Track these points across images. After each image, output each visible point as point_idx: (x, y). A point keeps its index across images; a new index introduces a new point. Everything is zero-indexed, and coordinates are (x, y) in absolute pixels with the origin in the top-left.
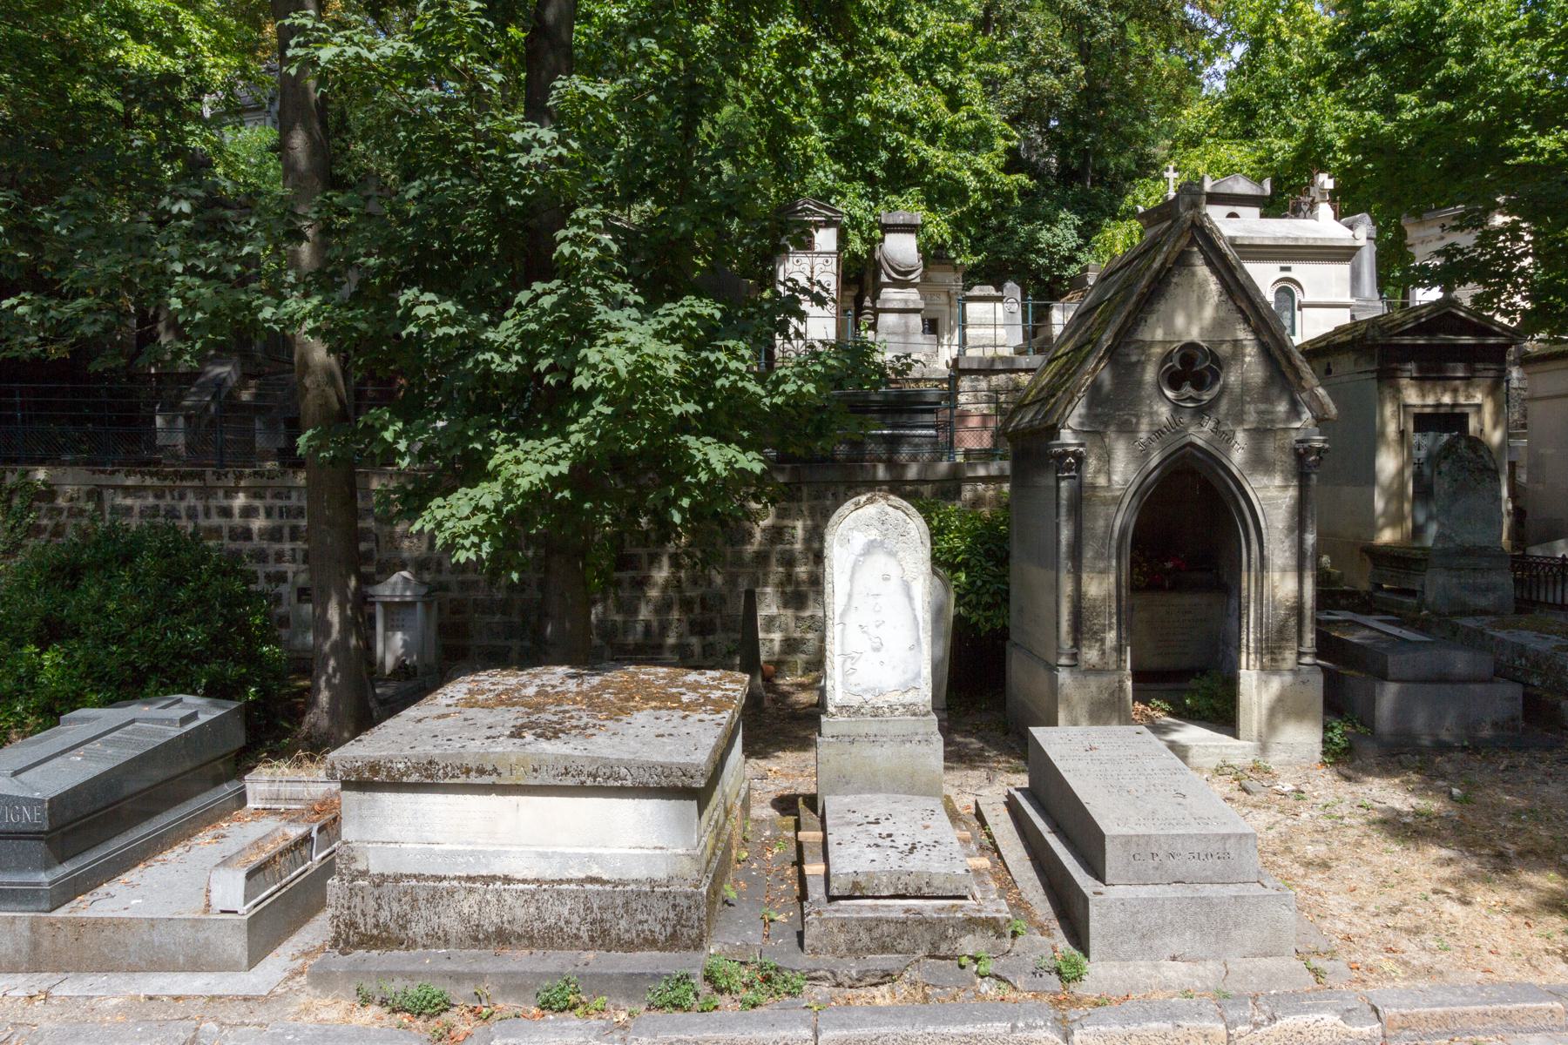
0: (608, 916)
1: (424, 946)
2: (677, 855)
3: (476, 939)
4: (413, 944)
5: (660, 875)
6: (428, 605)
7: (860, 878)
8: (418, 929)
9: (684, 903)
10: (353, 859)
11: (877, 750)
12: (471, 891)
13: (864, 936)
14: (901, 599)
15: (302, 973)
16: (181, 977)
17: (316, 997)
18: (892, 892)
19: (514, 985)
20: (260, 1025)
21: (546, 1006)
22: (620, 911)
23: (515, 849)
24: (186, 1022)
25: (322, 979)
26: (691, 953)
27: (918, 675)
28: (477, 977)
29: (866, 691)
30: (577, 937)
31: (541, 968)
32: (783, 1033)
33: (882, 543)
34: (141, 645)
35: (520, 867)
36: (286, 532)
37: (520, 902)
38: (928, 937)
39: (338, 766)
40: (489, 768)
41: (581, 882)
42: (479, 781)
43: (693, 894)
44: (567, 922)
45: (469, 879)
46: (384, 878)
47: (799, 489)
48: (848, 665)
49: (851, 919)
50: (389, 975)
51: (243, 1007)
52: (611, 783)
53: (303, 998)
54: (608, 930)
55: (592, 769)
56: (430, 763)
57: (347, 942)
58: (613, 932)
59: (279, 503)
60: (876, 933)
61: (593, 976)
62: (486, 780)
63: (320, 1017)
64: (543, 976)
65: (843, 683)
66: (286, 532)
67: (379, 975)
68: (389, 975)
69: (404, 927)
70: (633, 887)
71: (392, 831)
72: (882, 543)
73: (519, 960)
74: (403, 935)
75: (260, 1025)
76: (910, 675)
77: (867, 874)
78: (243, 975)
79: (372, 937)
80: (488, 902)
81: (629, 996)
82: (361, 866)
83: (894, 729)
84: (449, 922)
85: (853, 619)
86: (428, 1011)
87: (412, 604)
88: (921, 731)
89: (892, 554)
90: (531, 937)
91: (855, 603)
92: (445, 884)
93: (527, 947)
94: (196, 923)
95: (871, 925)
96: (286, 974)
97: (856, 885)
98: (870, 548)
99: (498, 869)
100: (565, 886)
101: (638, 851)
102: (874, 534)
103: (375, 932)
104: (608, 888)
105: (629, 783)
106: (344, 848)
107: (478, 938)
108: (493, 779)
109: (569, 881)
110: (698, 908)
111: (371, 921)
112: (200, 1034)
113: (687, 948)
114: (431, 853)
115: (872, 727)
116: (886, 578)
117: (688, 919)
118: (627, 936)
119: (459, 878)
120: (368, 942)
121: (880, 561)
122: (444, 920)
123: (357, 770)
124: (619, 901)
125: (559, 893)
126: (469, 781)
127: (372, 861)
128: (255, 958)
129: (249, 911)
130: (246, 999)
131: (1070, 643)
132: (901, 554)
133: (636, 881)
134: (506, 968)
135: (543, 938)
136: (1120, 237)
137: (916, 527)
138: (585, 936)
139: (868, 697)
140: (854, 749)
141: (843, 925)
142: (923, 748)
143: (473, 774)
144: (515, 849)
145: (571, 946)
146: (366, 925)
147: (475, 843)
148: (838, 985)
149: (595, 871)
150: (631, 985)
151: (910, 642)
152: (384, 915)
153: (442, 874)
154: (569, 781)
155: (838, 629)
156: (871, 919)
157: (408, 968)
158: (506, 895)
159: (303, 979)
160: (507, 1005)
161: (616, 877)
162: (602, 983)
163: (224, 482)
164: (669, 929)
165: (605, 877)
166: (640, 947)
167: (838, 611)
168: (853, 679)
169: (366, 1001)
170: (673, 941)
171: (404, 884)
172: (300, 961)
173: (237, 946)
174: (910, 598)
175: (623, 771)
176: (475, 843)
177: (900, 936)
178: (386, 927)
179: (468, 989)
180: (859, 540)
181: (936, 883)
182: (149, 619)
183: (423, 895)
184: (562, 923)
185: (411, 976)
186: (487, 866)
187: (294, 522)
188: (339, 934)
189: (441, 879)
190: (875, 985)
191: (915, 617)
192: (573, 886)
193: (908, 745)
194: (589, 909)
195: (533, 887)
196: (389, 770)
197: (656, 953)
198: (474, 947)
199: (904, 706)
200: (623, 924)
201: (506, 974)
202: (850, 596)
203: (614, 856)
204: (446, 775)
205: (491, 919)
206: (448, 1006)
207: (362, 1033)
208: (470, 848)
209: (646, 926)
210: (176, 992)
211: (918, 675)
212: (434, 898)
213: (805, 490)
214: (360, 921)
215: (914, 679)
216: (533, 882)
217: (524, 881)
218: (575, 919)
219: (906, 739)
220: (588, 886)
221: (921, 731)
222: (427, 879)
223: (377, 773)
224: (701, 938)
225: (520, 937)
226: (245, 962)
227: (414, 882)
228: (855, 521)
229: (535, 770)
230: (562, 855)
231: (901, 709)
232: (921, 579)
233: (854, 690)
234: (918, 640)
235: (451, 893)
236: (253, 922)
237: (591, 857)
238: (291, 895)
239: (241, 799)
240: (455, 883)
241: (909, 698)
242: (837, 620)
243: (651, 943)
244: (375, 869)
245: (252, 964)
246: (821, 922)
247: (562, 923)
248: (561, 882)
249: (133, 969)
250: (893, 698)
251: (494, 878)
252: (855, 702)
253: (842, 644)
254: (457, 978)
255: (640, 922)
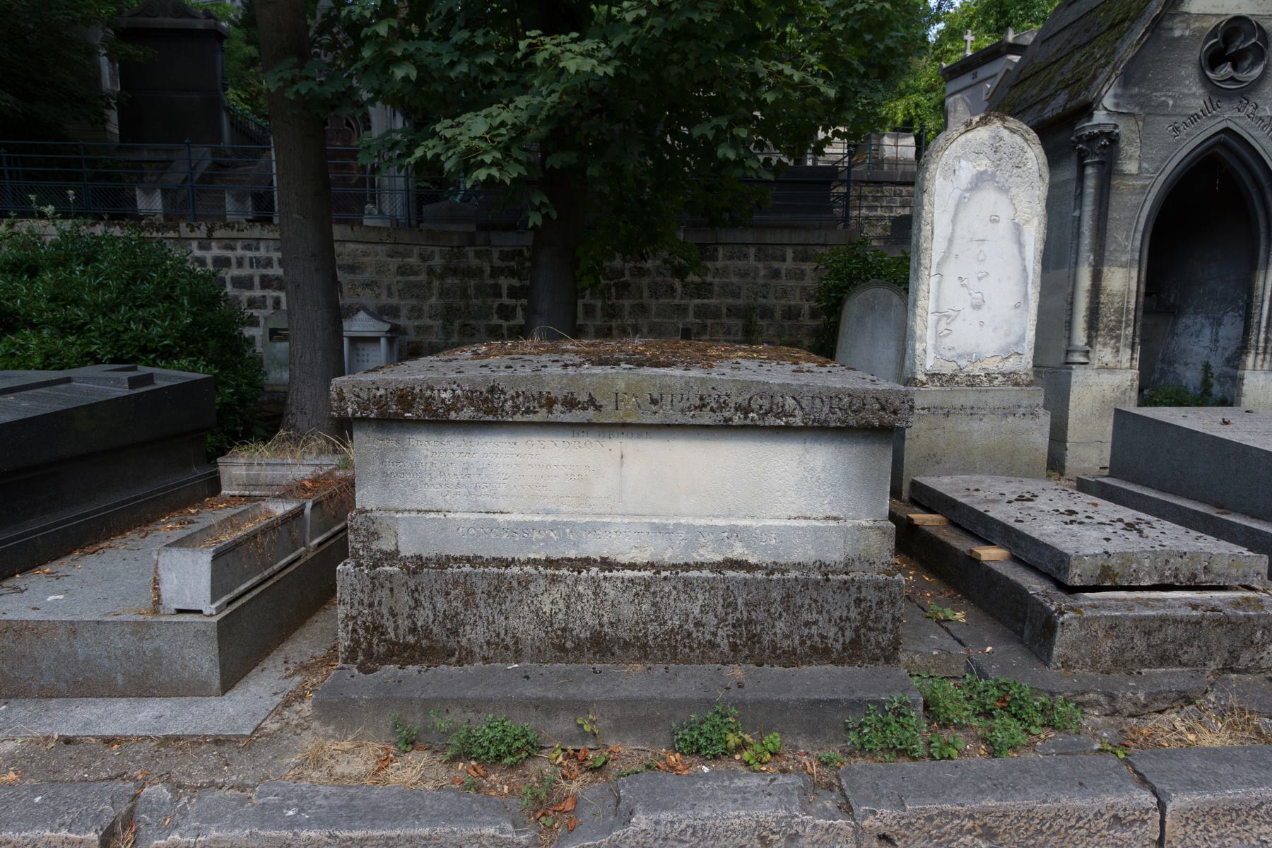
0: (759, 615)
1: (485, 659)
2: (861, 528)
3: (562, 648)
4: (466, 657)
5: (835, 556)
6: (390, 341)
7: (1113, 562)
8: (475, 635)
9: (871, 595)
10: (375, 535)
11: (975, 425)
12: (554, 580)
13: (1140, 643)
14: (1010, 247)
15: (302, 698)
16: (121, 705)
17: (327, 737)
18: (1155, 580)
19: (635, 717)
20: (242, 787)
21: (696, 751)
22: (777, 608)
23: (618, 520)
24: (119, 785)
25: (336, 711)
26: (881, 667)
27: (1022, 338)
28: (578, 706)
29: (960, 356)
30: (712, 645)
31: (674, 693)
32: (1110, 800)
33: (993, 175)
34: (102, 335)
35: (625, 547)
36: (257, 281)
37: (629, 596)
38: (1226, 643)
39: (347, 395)
40: (584, 398)
41: (717, 567)
42: (567, 418)
43: (887, 584)
44: (698, 624)
45: (549, 562)
46: (420, 563)
47: (716, 250)
48: (943, 325)
49: (1126, 618)
50: (444, 705)
51: (212, 757)
52: (771, 421)
53: (308, 741)
54: (759, 636)
55: (742, 400)
56: (492, 390)
57: (369, 654)
58: (766, 639)
59: (249, 254)
60: (1156, 639)
61: (759, 703)
62: (577, 416)
63: (338, 770)
64: (687, 704)
65: (935, 347)
66: (257, 281)
67: (426, 705)
68: (444, 705)
69: (454, 632)
70: (792, 574)
71: (433, 494)
72: (993, 175)
73: (633, 680)
74: (452, 643)
75: (242, 787)
76: (1013, 338)
77: (1122, 555)
78: (214, 702)
79: (407, 646)
80: (580, 596)
81: (814, 732)
82: (387, 546)
83: (993, 400)
84: (522, 624)
85: (951, 271)
86: (508, 760)
87: (376, 340)
88: (1025, 403)
89: (1004, 190)
90: (645, 646)
91: (955, 250)
92: (515, 570)
93: (637, 660)
94: (139, 629)
95: (1148, 627)
96: (278, 699)
97: (1106, 571)
98: (979, 181)
99: (594, 548)
100: (694, 574)
101: (803, 523)
102: (984, 164)
103: (411, 639)
104: (759, 575)
105: (798, 421)
106: (360, 519)
107: (566, 646)
108: (590, 414)
109: (699, 566)
110: (893, 604)
111: (404, 624)
112: (141, 806)
113: (874, 659)
114: (493, 526)
115: (968, 398)
116: (994, 220)
117: (877, 620)
118: (785, 644)
119: (534, 562)
120: (402, 653)
121: (989, 199)
122: (513, 622)
123: (378, 402)
124: (776, 594)
125: (687, 583)
126: (552, 418)
127: (403, 539)
128: (230, 680)
129: (219, 610)
130: (218, 741)
131: (1085, 340)
132: (1014, 191)
133: (798, 566)
134: (622, 693)
135: (661, 647)
136: (901, 107)
137: (1034, 155)
138: (724, 644)
139: (963, 363)
140: (948, 424)
141: (1113, 626)
142: (1026, 423)
143: (558, 407)
144: (618, 520)
145: (704, 659)
146: (398, 629)
147: (558, 512)
148: (1114, 713)
149: (738, 551)
150: (817, 717)
151: (1017, 298)
152: (424, 616)
153: (508, 555)
154: (706, 418)
155: (934, 280)
156: (1153, 619)
157: (469, 694)
158: (607, 586)
159: (306, 707)
160: (626, 748)
161: (769, 560)
162: (764, 714)
163: (197, 234)
164: (849, 634)
165: (753, 560)
166: (806, 659)
167: (936, 258)
168: (947, 342)
169: (411, 743)
170: (854, 651)
171: (453, 570)
172: (298, 679)
173: (204, 660)
174: (1020, 245)
175: (790, 402)
176: (558, 512)
177: (1189, 642)
178: (428, 633)
179: (563, 724)
180: (967, 170)
181: (1216, 568)
182: (113, 307)
183: (482, 586)
184: (690, 626)
185: (475, 705)
186: (575, 545)
187: (264, 272)
188: (356, 642)
189: (508, 563)
190: (1160, 712)
191: (1025, 269)
192: (706, 573)
193: (1010, 419)
194: (730, 605)
195: (647, 574)
196: (428, 402)
197: (830, 667)
198: (559, 660)
199: (1004, 375)
200: (781, 626)
201: (622, 702)
202: (951, 241)
203: (767, 530)
204: (516, 408)
205: (585, 618)
206: (533, 749)
207: (410, 805)
208: (550, 518)
209: (814, 630)
210: (108, 731)
211: (1022, 338)
212: (498, 589)
213: (721, 250)
214: (389, 623)
215: (1017, 344)
216: (645, 567)
217: (632, 566)
218: (711, 620)
219: (1008, 412)
220: (730, 574)
221: (1025, 403)
222: (486, 563)
223: (409, 406)
224: (896, 645)
225: (626, 645)
226: (216, 682)
227: (467, 568)
228: (963, 148)
229: (654, 402)
230: (690, 528)
231: (1001, 378)
232: (1035, 222)
233: (948, 354)
234: (1026, 296)
235: (525, 582)
236: (226, 628)
237: (735, 532)
238: (280, 596)
239: (214, 485)
240: (529, 569)
241: (1010, 365)
242: (933, 272)
243: (822, 653)
244: (407, 550)
245: (227, 686)
246: (1083, 622)
247: (690, 626)
248: (687, 567)
249: (48, 693)
250: (991, 365)
251: (587, 562)
252: (948, 369)
253: (938, 299)
254: (548, 708)
255: (807, 624)
